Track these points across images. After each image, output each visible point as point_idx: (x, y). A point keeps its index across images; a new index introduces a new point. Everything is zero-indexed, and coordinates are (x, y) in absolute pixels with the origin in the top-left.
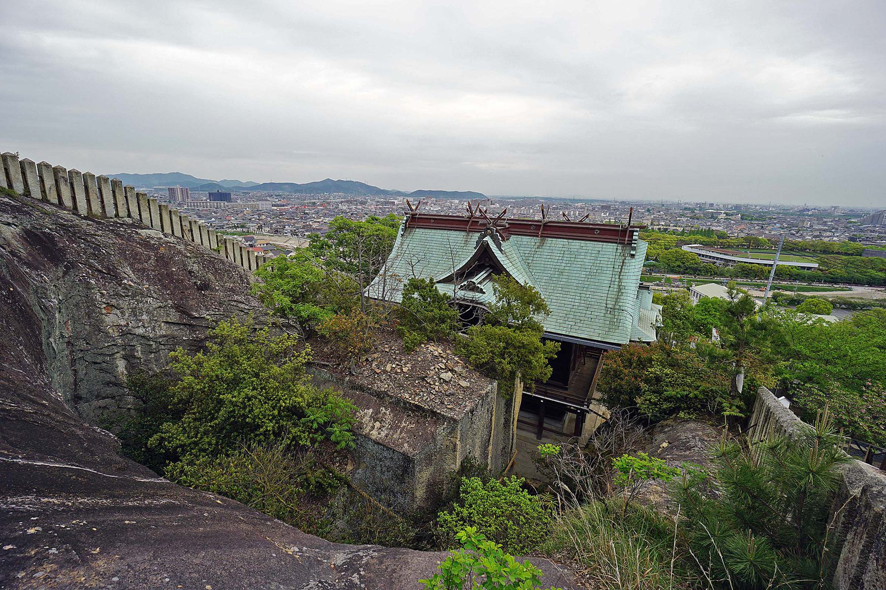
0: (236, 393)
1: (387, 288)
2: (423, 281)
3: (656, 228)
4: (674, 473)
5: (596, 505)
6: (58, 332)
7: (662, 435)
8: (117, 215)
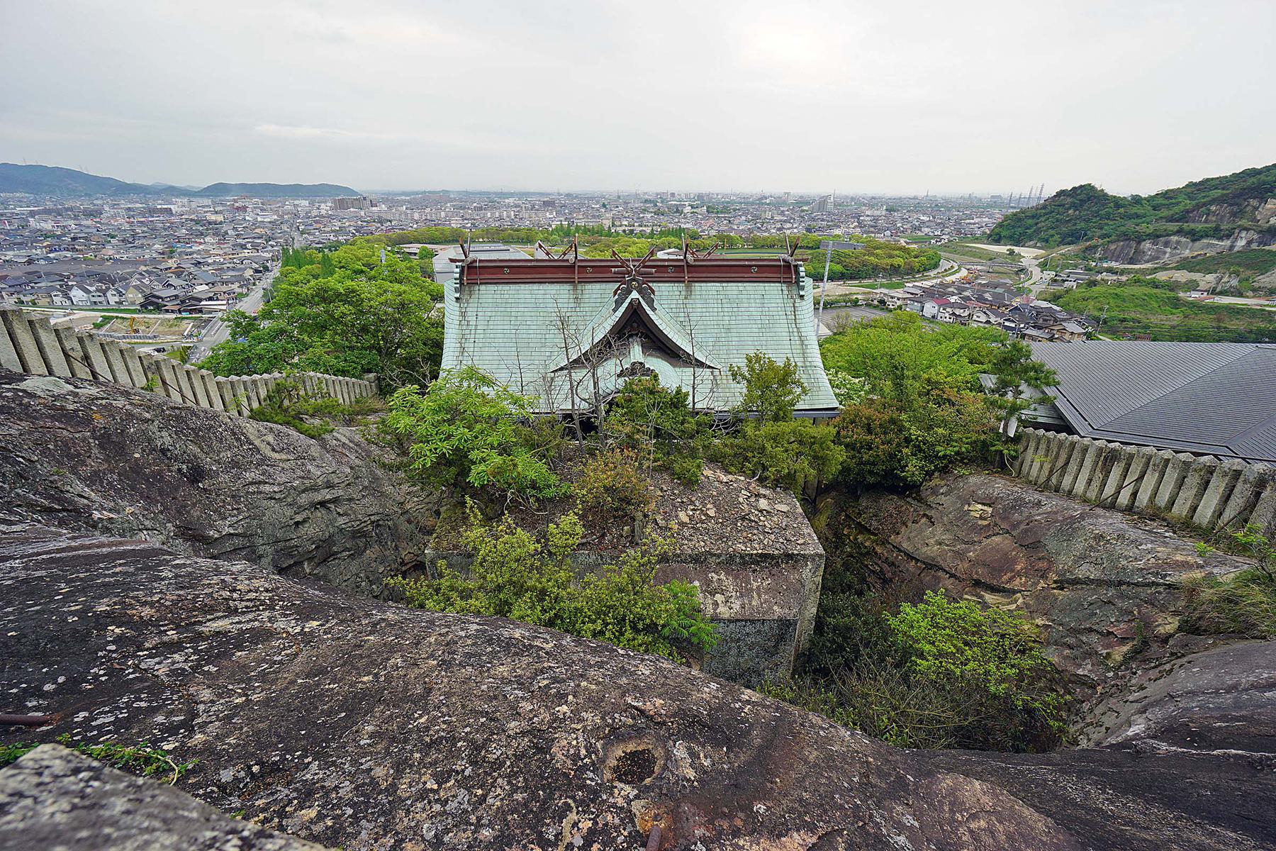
3: (620, 229)
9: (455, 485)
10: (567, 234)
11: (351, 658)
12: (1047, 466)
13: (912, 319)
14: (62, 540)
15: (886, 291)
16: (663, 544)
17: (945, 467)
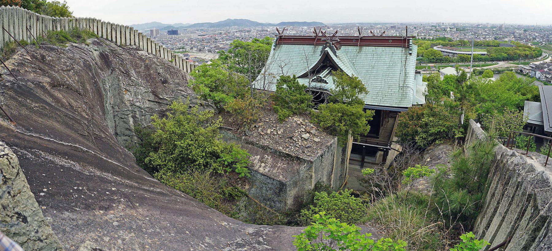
0: (183, 142)
1: (267, 82)
2: (289, 77)
4: (432, 172)
5: (392, 196)
6: (110, 100)
7: (427, 155)
8: (130, 44)
15: (522, 66)
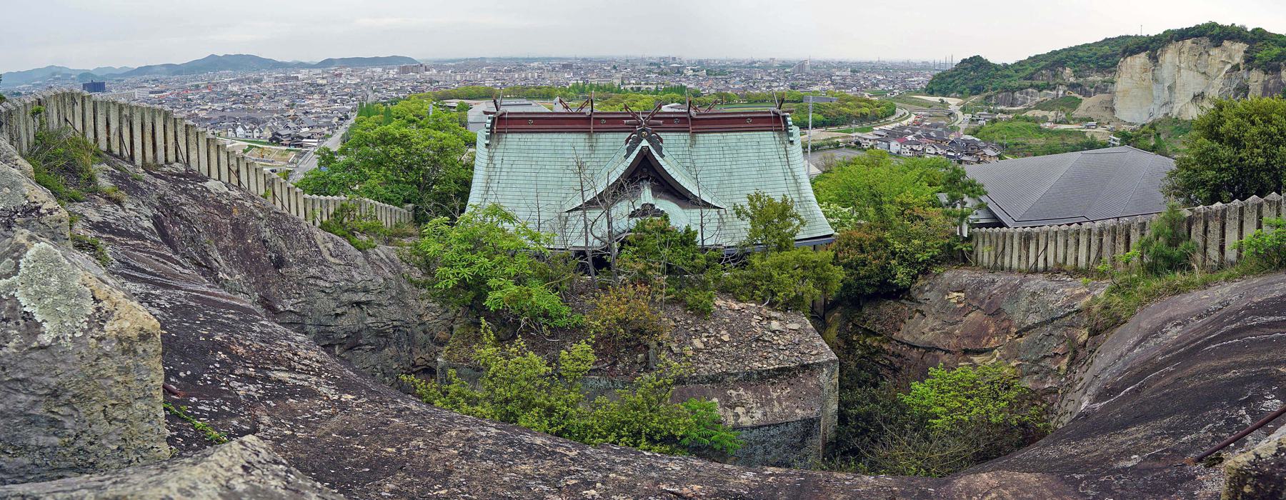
3: (628, 87)
9: (471, 307)
10: (582, 91)
11: (378, 430)
12: (993, 253)
13: (882, 155)
14: (204, 287)
16: (677, 368)
17: (925, 269)
